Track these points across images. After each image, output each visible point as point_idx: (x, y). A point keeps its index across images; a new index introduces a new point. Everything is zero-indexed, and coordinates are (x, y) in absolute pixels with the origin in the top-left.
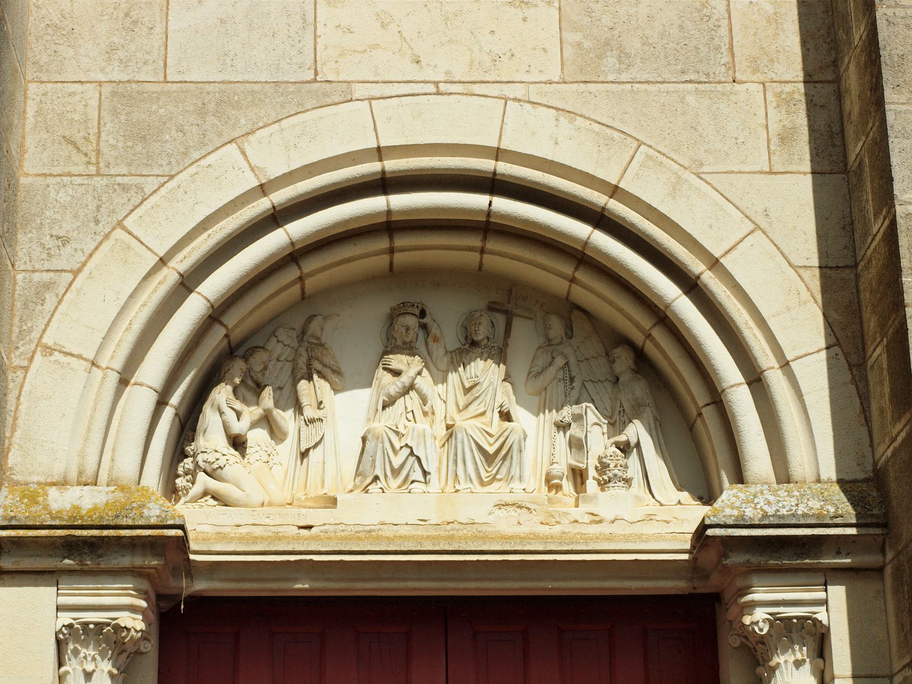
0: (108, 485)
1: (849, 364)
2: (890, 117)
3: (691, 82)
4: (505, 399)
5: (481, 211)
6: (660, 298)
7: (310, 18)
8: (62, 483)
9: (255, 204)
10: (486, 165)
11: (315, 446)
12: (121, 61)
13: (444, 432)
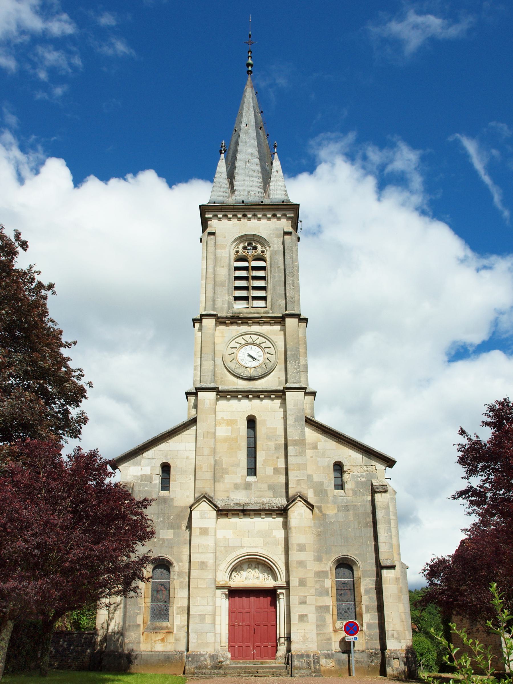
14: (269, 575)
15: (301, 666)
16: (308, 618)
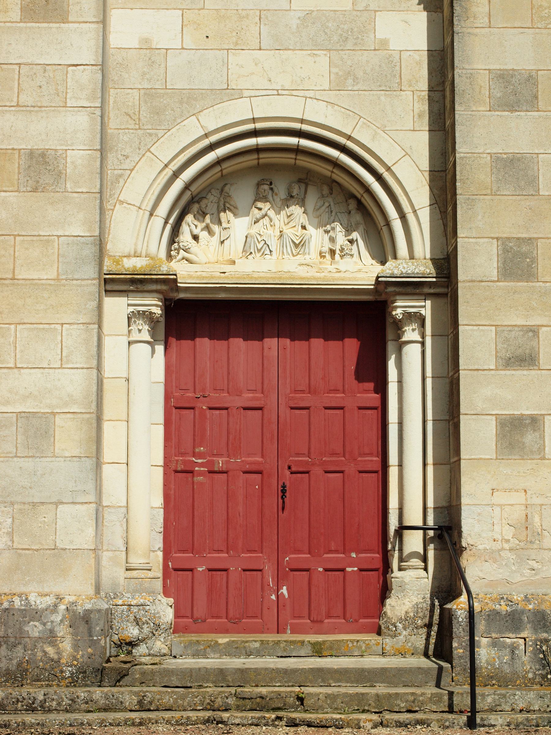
0: (146, 257)
1: (440, 211)
2: (457, 117)
3: (383, 90)
4: (304, 220)
5: (295, 145)
6: (367, 182)
7: (226, 61)
8: (128, 256)
9: (203, 142)
10: (297, 126)
11: (226, 239)
12: (148, 79)
13: (279, 234)
14: (355, 235)
15: (507, 669)
16: (542, 437)
